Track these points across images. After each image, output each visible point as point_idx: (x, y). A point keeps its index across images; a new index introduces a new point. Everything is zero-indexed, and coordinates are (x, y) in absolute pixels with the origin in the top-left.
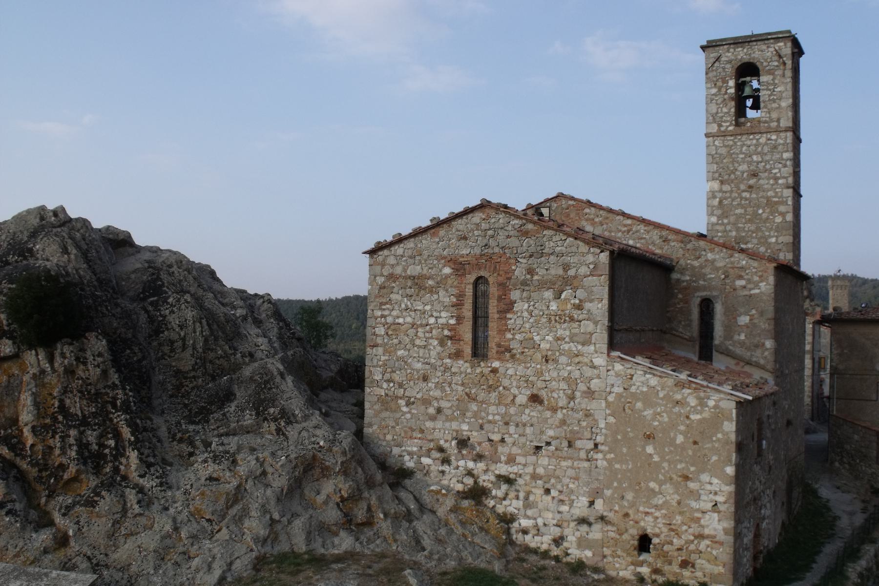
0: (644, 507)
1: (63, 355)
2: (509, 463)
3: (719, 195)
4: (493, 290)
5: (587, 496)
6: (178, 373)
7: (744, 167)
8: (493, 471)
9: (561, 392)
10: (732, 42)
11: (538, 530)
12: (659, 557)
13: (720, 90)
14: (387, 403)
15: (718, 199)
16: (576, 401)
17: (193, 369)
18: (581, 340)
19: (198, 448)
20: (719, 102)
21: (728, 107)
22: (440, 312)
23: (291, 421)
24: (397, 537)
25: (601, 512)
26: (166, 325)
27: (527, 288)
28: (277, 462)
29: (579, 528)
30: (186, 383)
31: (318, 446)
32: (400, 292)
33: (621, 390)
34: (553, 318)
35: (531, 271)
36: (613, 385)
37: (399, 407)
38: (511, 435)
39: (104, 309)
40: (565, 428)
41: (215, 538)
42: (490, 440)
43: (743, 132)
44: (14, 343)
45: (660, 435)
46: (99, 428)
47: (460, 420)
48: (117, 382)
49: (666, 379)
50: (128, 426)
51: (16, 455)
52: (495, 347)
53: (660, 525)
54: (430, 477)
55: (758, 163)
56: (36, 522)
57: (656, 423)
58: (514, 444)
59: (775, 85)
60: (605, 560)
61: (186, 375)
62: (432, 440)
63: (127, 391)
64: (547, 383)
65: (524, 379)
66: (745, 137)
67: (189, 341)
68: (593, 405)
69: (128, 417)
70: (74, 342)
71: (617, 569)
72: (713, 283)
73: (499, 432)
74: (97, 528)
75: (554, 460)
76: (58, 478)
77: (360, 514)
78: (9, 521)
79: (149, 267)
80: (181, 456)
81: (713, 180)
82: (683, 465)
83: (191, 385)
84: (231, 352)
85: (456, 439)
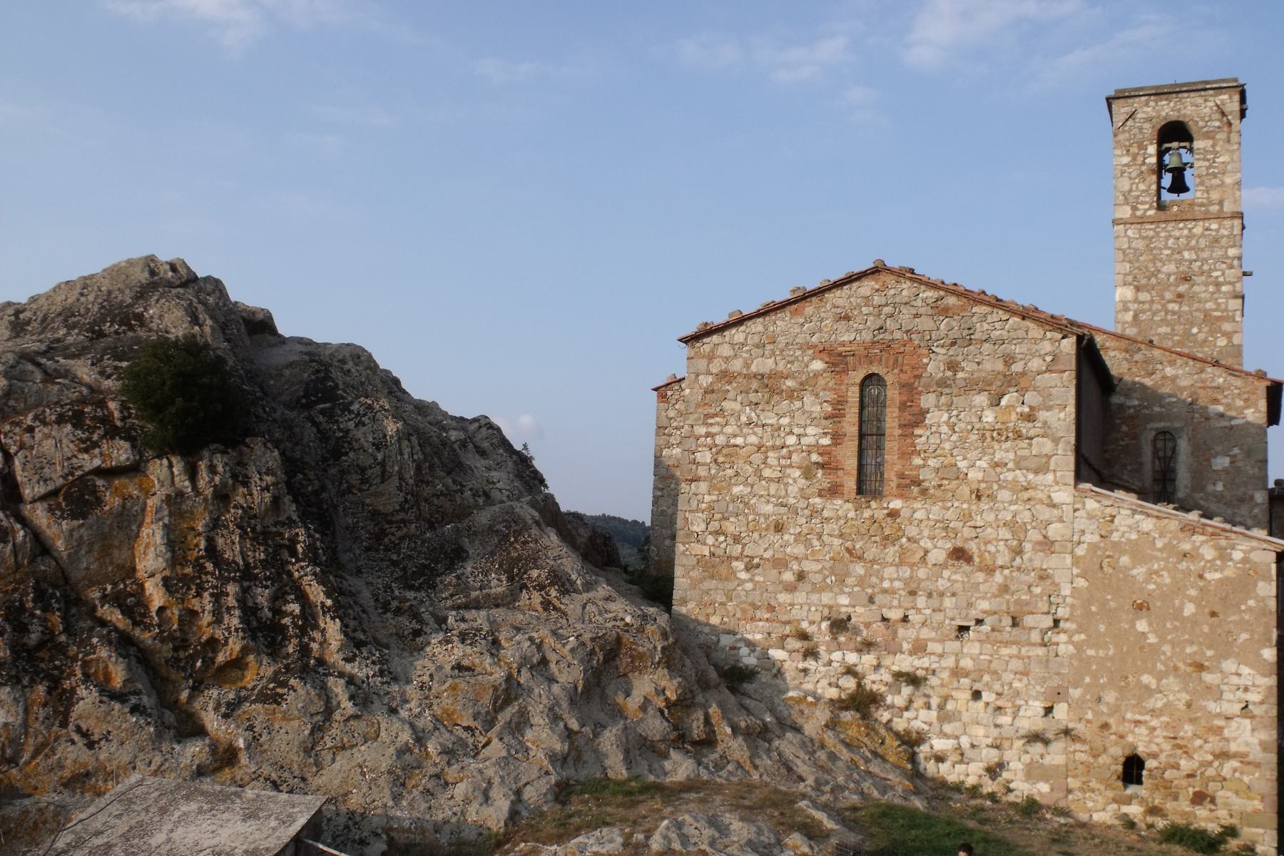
0: (1134, 713)
1: (212, 469)
2: (916, 654)
3: (1134, 307)
4: (893, 394)
5: (1042, 698)
6: (375, 514)
7: (1171, 267)
8: (887, 667)
9: (1002, 543)
10: (1154, 92)
11: (962, 755)
12: (1157, 789)
13: (1134, 159)
14: (714, 566)
15: (1131, 313)
16: (1026, 557)
17: (402, 509)
18: (1033, 466)
19: (427, 624)
20: (1133, 175)
21: (1147, 183)
22: (805, 427)
23: (566, 590)
24: (757, 762)
25: (1065, 723)
26: (350, 443)
27: (947, 390)
28: (564, 645)
29: (1028, 748)
30: (392, 530)
31: (623, 623)
32: (739, 398)
33: (1096, 538)
34: (988, 434)
35: (953, 366)
36: (1083, 532)
37: (734, 573)
38: (919, 611)
39: (261, 411)
40: (1007, 597)
41: (481, 756)
42: (884, 619)
43: (1169, 218)
44: (133, 447)
45: (1159, 604)
46: (272, 584)
47: (836, 590)
48: (295, 517)
49: (1166, 521)
50: (321, 583)
51: (136, 624)
52: (894, 478)
53: (1159, 740)
54: (784, 680)
55: (1191, 262)
56: (175, 728)
57: (1152, 587)
58: (923, 624)
59: (1216, 153)
60: (1070, 797)
61: (389, 518)
62: (788, 622)
63: (312, 532)
64: (978, 530)
65: (941, 525)
66: (1171, 225)
67: (393, 467)
68: (1051, 563)
69: (318, 569)
70: (229, 450)
71: (1090, 811)
72: (1175, 410)
73: (900, 606)
74: (285, 737)
75: (989, 646)
76: (209, 662)
77: (696, 728)
78: (136, 722)
79: (311, 361)
80: (400, 637)
81: (1125, 285)
82: (1195, 648)
83: (399, 534)
84: (455, 488)
85: (829, 619)
